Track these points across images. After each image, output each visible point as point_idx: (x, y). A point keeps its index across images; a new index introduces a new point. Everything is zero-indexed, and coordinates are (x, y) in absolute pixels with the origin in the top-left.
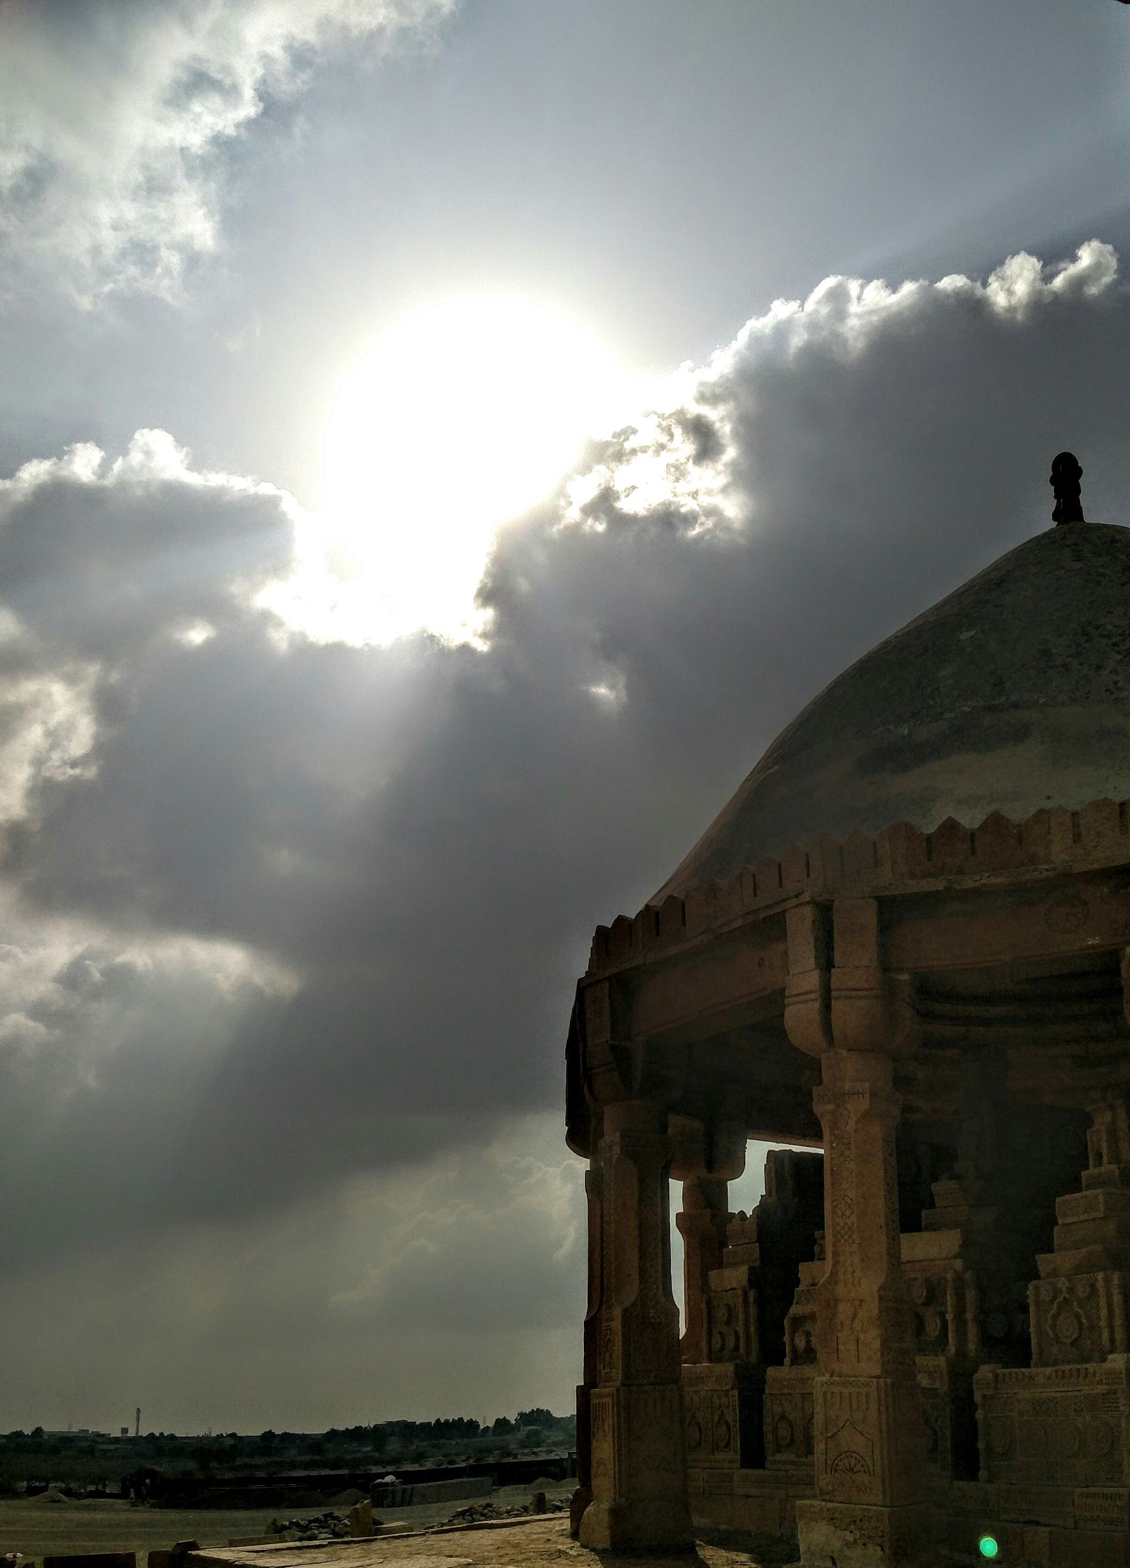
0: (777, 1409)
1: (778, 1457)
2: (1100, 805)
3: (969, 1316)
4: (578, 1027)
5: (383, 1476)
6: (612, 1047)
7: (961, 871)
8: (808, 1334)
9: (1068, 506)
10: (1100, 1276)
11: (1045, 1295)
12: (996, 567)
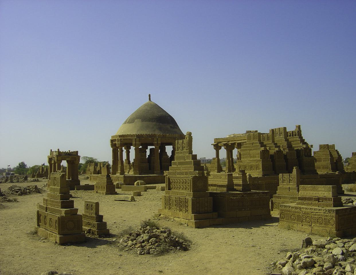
9: (150, 99)
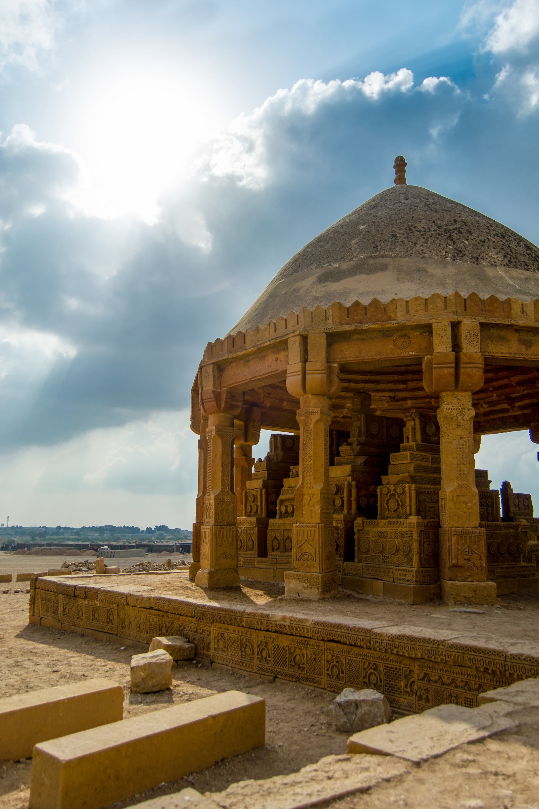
0: (273, 535)
1: (273, 553)
2: (417, 299)
3: (353, 499)
4: (199, 382)
5: (103, 546)
6: (213, 391)
7: (361, 323)
8: (286, 507)
9: (400, 179)
10: (407, 485)
11: (385, 490)
12: (373, 200)
